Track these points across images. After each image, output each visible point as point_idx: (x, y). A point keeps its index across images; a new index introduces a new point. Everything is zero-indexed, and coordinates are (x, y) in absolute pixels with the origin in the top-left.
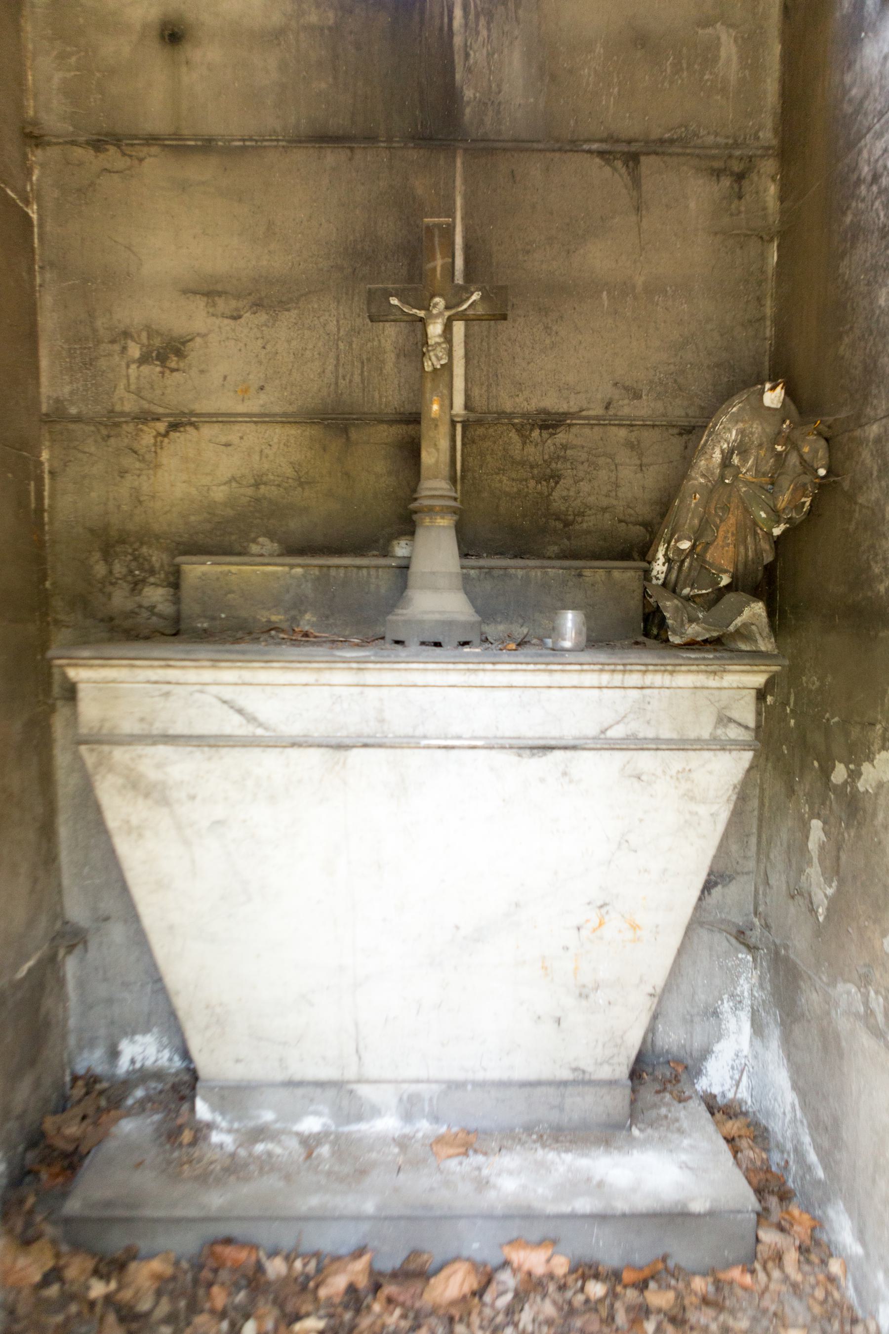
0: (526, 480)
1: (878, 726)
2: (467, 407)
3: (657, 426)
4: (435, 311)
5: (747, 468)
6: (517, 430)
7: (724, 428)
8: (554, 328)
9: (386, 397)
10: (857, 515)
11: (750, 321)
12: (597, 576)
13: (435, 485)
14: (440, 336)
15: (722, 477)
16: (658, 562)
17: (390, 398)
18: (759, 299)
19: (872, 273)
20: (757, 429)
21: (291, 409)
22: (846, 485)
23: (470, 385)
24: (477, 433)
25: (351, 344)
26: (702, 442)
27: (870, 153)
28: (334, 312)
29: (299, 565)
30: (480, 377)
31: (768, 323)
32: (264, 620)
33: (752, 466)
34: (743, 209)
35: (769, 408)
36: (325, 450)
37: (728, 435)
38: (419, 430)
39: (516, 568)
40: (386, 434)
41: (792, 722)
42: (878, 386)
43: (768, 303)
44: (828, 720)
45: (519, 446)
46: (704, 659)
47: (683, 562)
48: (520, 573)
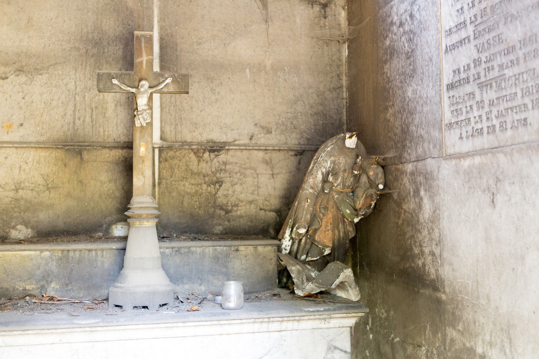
0: (201, 184)
1: (423, 348)
2: (161, 138)
3: (282, 150)
4: (142, 90)
5: (337, 183)
6: (194, 153)
7: (323, 160)
8: (217, 90)
9: (108, 131)
10: (403, 215)
11: (334, 88)
12: (248, 250)
13: (143, 200)
14: (145, 105)
15: (323, 189)
16: (286, 239)
17: (111, 132)
18: (338, 76)
19: (403, 77)
20: (343, 161)
21: (42, 139)
22: (395, 196)
23: (163, 125)
24: (169, 155)
25: (84, 97)
26: (310, 168)
27: (397, 9)
28: (73, 76)
29: (47, 250)
30: (170, 120)
31: (344, 89)
32: (21, 289)
33: (341, 182)
34: (327, 24)
35: (349, 148)
36: (65, 166)
37: (325, 164)
38: (132, 153)
39: (196, 247)
40: (107, 155)
41: (371, 336)
42: (411, 142)
43: (344, 78)
44: (393, 339)
45: (196, 162)
46: (318, 311)
47: (301, 240)
48: (199, 250)
